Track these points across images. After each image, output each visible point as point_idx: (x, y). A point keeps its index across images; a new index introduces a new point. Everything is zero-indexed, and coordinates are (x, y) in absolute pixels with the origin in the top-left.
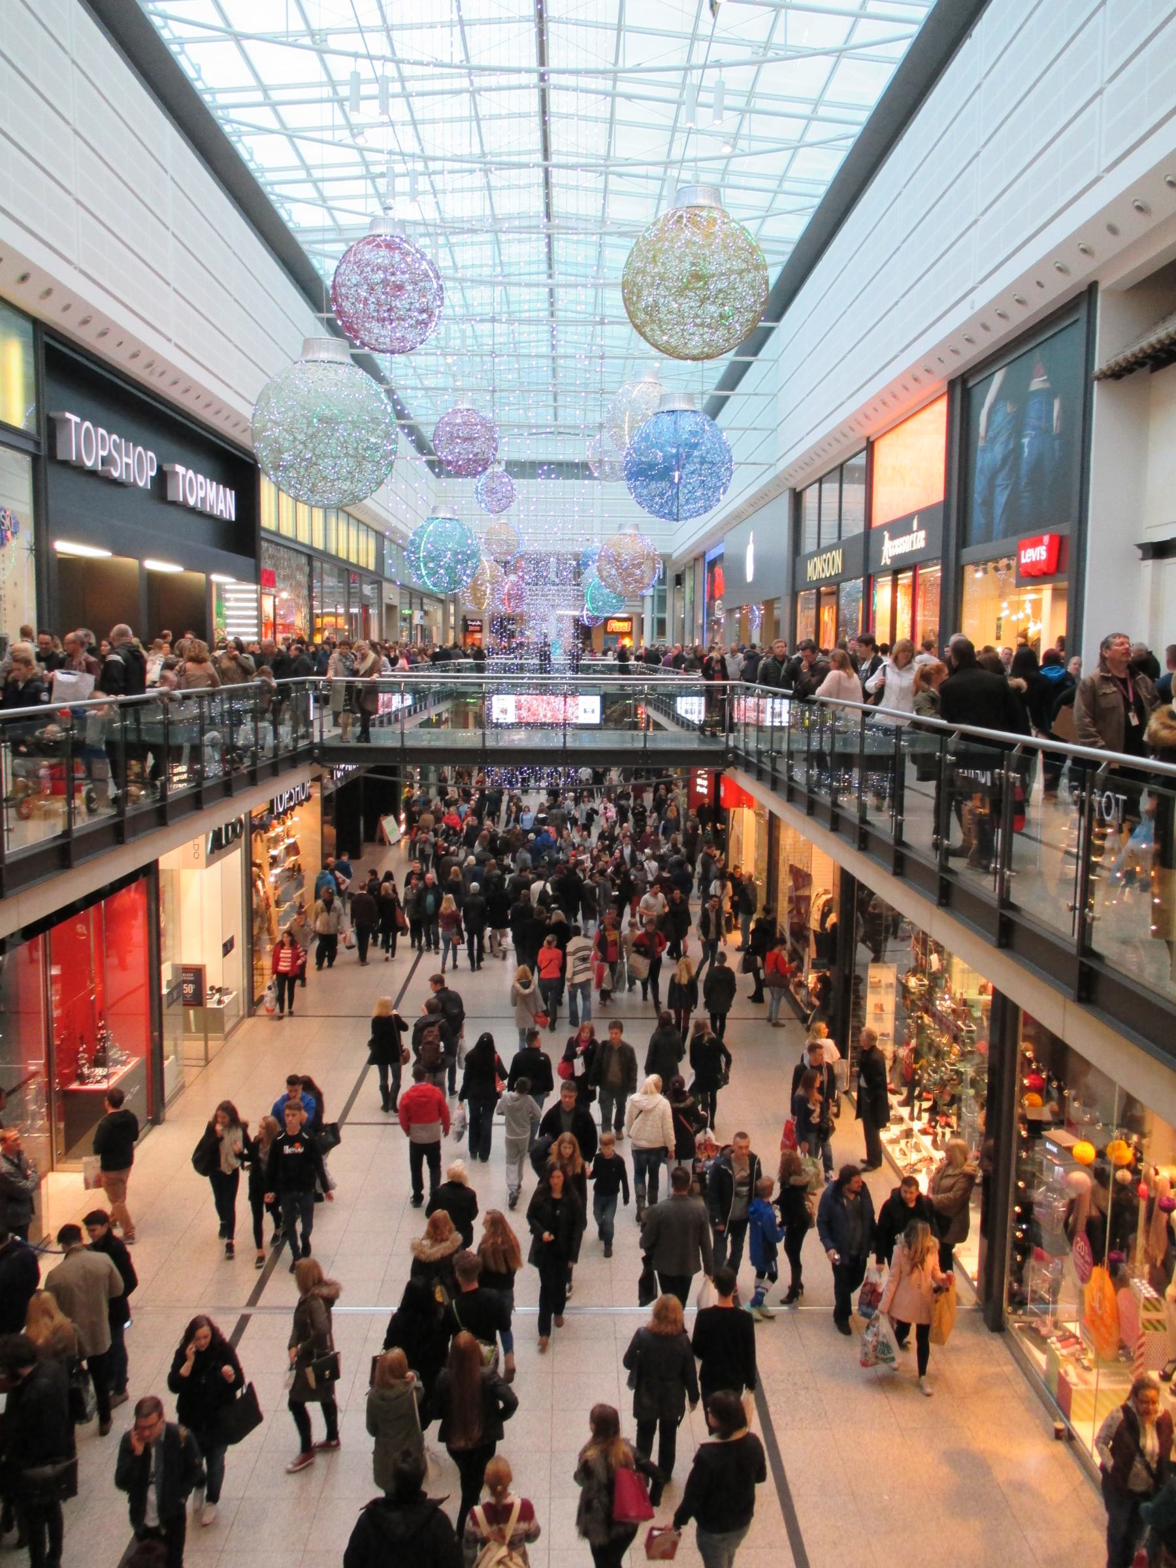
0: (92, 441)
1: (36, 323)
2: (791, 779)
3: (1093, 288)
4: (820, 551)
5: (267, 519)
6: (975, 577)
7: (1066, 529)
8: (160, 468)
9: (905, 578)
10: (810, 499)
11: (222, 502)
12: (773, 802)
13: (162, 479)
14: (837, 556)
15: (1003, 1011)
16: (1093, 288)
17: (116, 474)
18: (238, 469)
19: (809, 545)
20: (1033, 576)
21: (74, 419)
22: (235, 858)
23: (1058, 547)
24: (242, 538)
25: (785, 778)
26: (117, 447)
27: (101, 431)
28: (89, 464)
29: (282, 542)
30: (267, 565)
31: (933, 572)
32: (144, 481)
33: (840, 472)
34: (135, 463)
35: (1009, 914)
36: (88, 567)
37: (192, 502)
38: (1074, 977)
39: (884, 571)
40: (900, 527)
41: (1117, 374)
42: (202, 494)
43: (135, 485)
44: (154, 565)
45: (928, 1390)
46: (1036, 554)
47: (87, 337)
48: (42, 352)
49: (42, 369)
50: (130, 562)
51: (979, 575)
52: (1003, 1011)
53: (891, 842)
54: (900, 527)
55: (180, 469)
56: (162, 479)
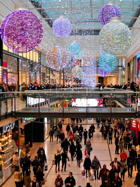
29: (8, 54)
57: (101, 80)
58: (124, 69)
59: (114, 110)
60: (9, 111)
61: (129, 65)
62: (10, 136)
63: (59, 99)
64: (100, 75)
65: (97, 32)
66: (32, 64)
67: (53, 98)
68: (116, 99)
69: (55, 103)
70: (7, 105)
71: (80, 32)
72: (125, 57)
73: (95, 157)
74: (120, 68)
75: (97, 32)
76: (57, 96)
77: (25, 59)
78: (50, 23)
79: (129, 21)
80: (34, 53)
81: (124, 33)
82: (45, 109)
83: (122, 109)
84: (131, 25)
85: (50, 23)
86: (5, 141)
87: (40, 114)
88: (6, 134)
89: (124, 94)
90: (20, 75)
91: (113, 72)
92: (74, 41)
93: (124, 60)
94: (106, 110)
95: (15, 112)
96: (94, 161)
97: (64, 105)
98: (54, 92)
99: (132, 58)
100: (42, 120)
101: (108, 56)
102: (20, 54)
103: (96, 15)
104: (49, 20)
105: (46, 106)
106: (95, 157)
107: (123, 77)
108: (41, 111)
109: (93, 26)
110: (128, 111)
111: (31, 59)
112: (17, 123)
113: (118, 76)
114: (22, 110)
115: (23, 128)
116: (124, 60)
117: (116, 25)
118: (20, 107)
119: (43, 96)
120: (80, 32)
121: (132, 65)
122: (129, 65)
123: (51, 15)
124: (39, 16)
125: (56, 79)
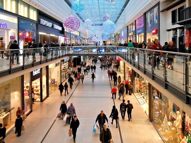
0: (44, 22)
1: (37, 9)
2: (128, 59)
3: (159, 2)
4: (130, 32)
5: (65, 30)
6: (148, 34)
7: (158, 28)
8: (52, 25)
9: (140, 35)
10: (129, 27)
11: (60, 29)
12: (124, 61)
13: (53, 26)
14: (132, 33)
15: (150, 85)
16: (159, 2)
17: (47, 25)
18: (61, 24)
19: (129, 32)
20: (154, 34)
21: (42, 20)
22: (59, 67)
23: (156, 31)
24: (62, 32)
25: (133, 62)
26: (47, 23)
27: (45, 21)
28: (44, 24)
29: (67, 33)
30: (65, 35)
31: (143, 34)
32: (51, 26)
33: (132, 24)
34: (49, 24)
35: (167, 83)
36: (44, 36)
37: (56, 28)
38: (152, 76)
39: (137, 34)
40: (139, 29)
41: (163, 11)
42: (57, 28)
43: (49, 27)
44: (51, 35)
45: (65, 35)
46: (154, 31)
47: (44, 11)
48: (38, 13)
49: (38, 15)
50: (49, 35)
51: (148, 34)
52: (150, 85)
53: (152, 74)
54: (139, 29)
55: (55, 25)
56: (53, 26)
57: (104, 42)
58: (113, 38)
59: (109, 53)
60: (67, 54)
61: (115, 36)
62: (67, 63)
63: (87, 49)
64: (104, 40)
65: (101, 25)
66: (76, 36)
67: (84, 49)
68: (110, 49)
69: (85, 51)
70: (65, 52)
71: (96, 25)
72: (114, 34)
73: (72, 105)
74: (112, 38)
75: (101, 25)
76: (86, 48)
77: (73, 34)
78: (83, 21)
79: (115, 21)
80: (76, 32)
81: (112, 25)
82: (81, 53)
83: (112, 52)
84: (115, 22)
85: (83, 21)
86: (65, 65)
87: (79, 55)
88: (66, 62)
89: (113, 47)
90: (72, 41)
91: (108, 39)
92: (93, 28)
93: (113, 35)
94: (106, 53)
95: (69, 54)
96: (69, 108)
97: (89, 51)
98: (83, 46)
99: (116, 34)
100: (80, 57)
101: (107, 33)
102: (72, 33)
103: (102, 19)
104: (10, 37)
105: (82, 52)
106: (72, 105)
107: (113, 41)
108: (79, 54)
109: (101, 23)
110: (115, 53)
111: (75, 34)
112: (70, 58)
113: (111, 41)
114: (72, 53)
115: (73, 60)
116: (113, 35)
117: (109, 22)
118: (71, 52)
119: (80, 48)
120: (96, 25)
121: (116, 37)
122: (115, 36)
123: (84, 18)
124: (79, 18)
125: (86, 42)
